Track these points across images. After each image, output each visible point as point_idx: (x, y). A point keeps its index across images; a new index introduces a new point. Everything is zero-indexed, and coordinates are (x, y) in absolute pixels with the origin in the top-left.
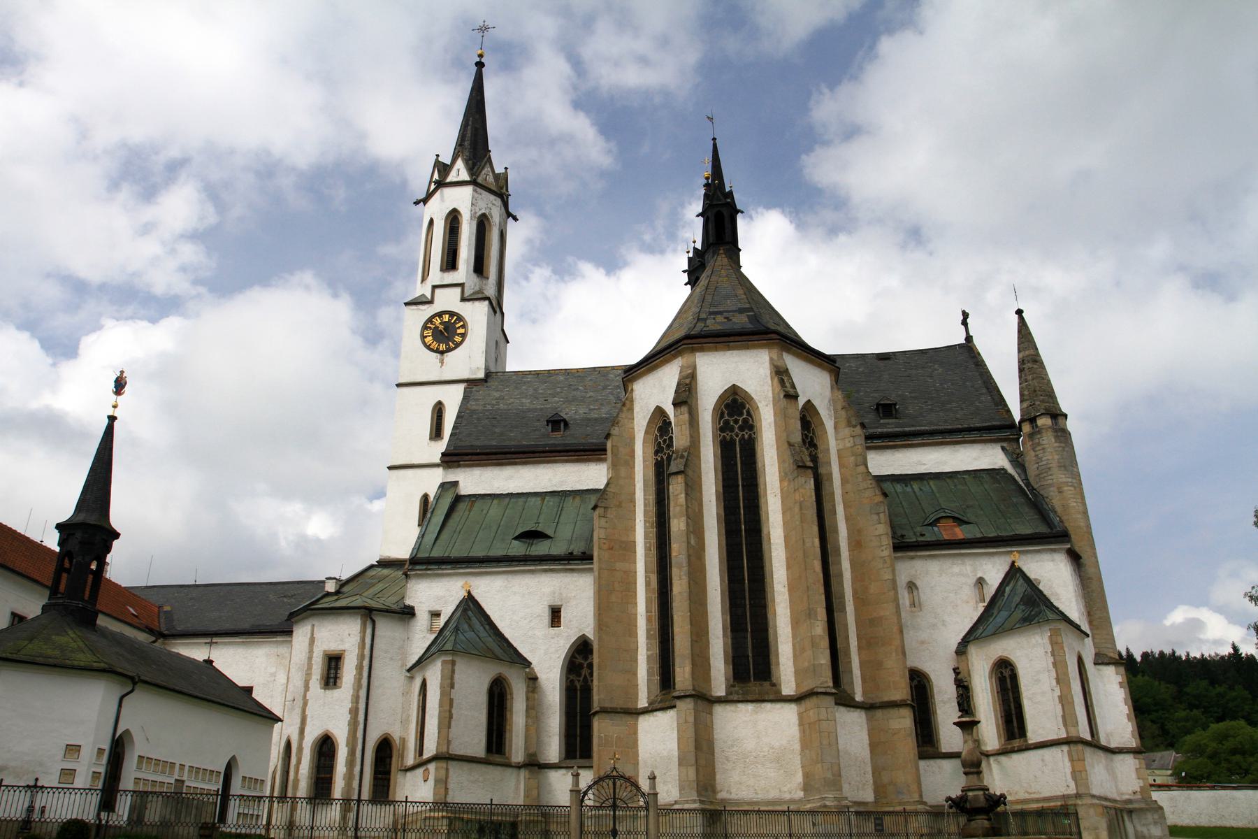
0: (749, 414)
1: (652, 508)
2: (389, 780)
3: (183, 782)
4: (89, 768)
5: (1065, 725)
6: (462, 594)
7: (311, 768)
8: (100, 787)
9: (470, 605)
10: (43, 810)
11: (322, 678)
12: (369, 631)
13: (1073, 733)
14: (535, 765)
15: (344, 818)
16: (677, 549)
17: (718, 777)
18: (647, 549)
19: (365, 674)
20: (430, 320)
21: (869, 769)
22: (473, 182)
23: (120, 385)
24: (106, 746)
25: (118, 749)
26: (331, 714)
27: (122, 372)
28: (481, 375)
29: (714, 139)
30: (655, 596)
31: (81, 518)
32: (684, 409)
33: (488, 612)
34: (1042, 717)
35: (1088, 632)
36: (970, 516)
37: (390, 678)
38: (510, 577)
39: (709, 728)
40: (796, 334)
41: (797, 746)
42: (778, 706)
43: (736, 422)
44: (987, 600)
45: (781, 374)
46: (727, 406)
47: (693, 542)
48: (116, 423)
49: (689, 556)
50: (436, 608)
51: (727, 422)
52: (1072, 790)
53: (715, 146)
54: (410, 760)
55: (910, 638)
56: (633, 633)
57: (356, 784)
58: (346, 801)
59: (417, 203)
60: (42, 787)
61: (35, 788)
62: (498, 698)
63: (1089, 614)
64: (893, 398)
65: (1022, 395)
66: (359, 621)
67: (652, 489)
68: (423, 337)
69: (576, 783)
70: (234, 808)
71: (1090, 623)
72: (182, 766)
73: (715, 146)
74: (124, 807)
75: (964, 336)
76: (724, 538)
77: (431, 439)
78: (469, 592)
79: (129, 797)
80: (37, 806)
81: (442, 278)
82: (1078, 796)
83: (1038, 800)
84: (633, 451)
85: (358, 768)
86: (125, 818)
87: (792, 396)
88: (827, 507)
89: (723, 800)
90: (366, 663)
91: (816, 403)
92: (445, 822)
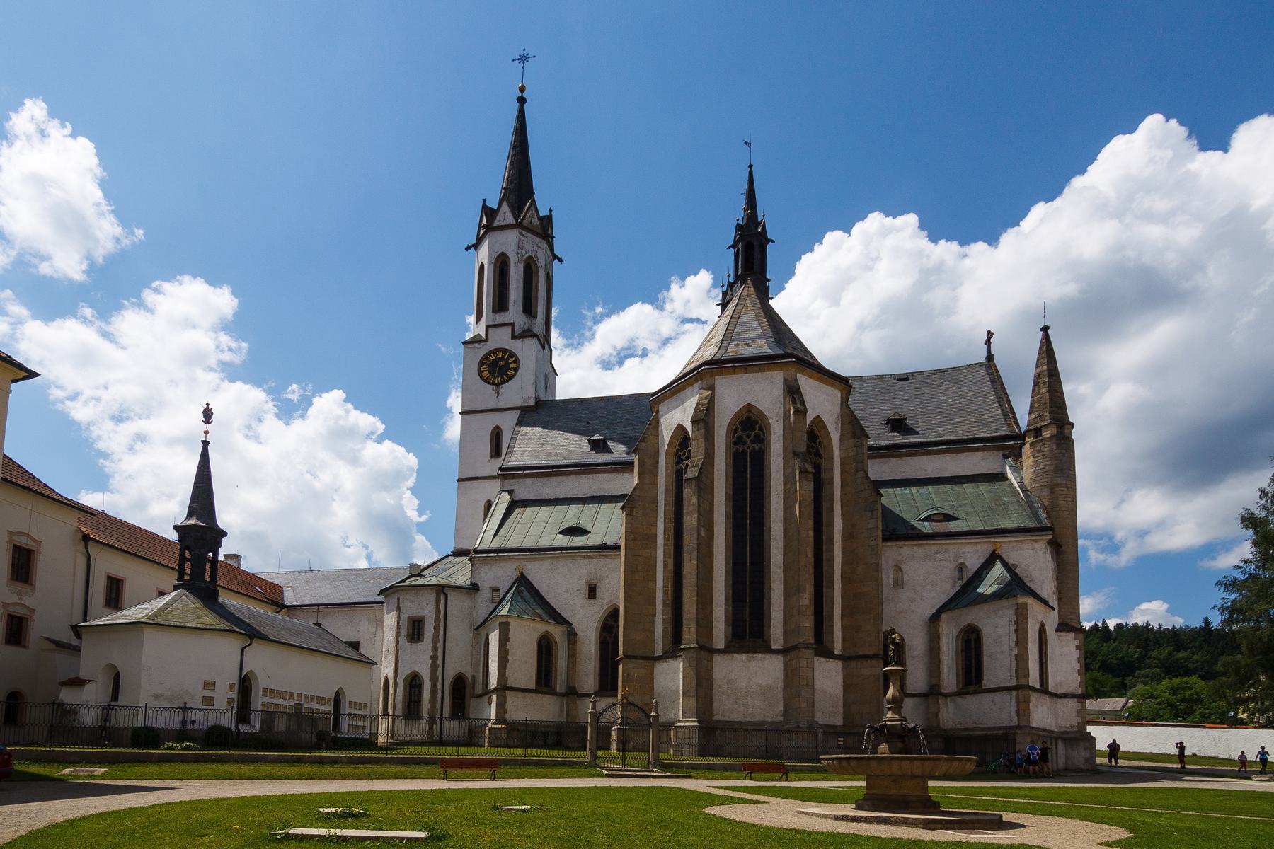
0: (761, 429)
1: (671, 508)
4: (224, 695)
5: (1017, 675)
12: (442, 602)
13: (1023, 681)
14: (572, 693)
15: (431, 728)
16: (690, 539)
17: (715, 705)
18: (666, 539)
19: (441, 632)
20: (486, 357)
21: (841, 704)
22: (519, 225)
24: (236, 682)
25: (245, 685)
28: (532, 403)
29: (751, 166)
30: (671, 575)
32: (701, 425)
34: (998, 668)
35: (1056, 606)
36: (960, 513)
37: (459, 633)
39: (709, 671)
40: (813, 357)
41: (781, 685)
42: (767, 656)
43: (748, 436)
44: (965, 579)
45: (793, 392)
46: (741, 423)
47: (703, 534)
49: (698, 545)
51: (740, 438)
52: (1015, 722)
53: (751, 173)
54: (479, 690)
55: (887, 610)
56: (653, 603)
57: (438, 706)
59: (468, 248)
61: (185, 708)
62: (545, 648)
63: (1060, 592)
64: (904, 413)
65: (1032, 407)
67: (672, 493)
68: (480, 372)
70: (345, 722)
71: (1059, 600)
72: (299, 695)
73: (751, 173)
75: (985, 353)
76: (730, 531)
77: (491, 457)
80: (189, 719)
81: (494, 319)
82: (1019, 727)
83: (983, 729)
84: (657, 462)
85: (439, 696)
87: (802, 412)
88: (825, 505)
89: (718, 721)
91: (825, 418)
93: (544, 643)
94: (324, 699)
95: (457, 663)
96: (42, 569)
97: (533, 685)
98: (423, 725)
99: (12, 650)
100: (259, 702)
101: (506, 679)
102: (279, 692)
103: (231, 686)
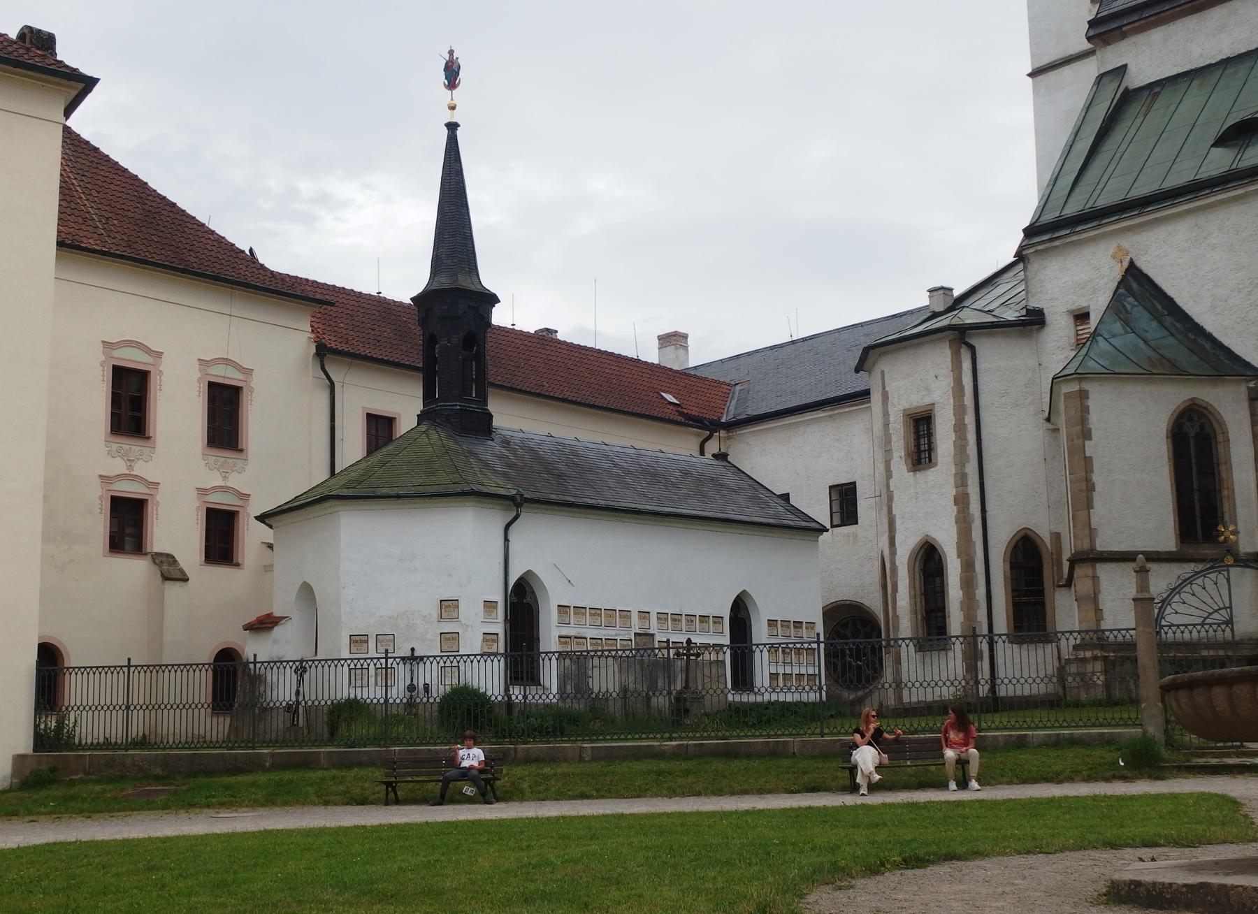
2: (1043, 604)
3: (653, 635)
4: (481, 627)
6: (1115, 272)
7: (913, 597)
8: (502, 650)
9: (1136, 283)
10: (427, 688)
11: (908, 454)
12: (966, 365)
15: (972, 668)
19: (971, 437)
23: (452, 73)
24: (498, 596)
25: (522, 604)
26: (925, 509)
27: (451, 52)
31: (444, 282)
33: (1171, 292)
38: (1202, 219)
48: (459, 132)
50: (1080, 303)
57: (982, 615)
58: (971, 637)
60: (422, 658)
66: (948, 352)
69: (1143, 586)
72: (644, 615)
74: (551, 673)
78: (1132, 263)
79: (554, 661)
85: (981, 591)
86: (554, 690)
90: (970, 419)
92: (1099, 666)
93: (1191, 431)
94: (704, 618)
95: (1024, 498)
96: (256, 420)
97: (1165, 537)
98: (953, 664)
99: (220, 573)
100: (551, 633)
101: (1092, 533)
102: (596, 611)
103: (489, 605)
